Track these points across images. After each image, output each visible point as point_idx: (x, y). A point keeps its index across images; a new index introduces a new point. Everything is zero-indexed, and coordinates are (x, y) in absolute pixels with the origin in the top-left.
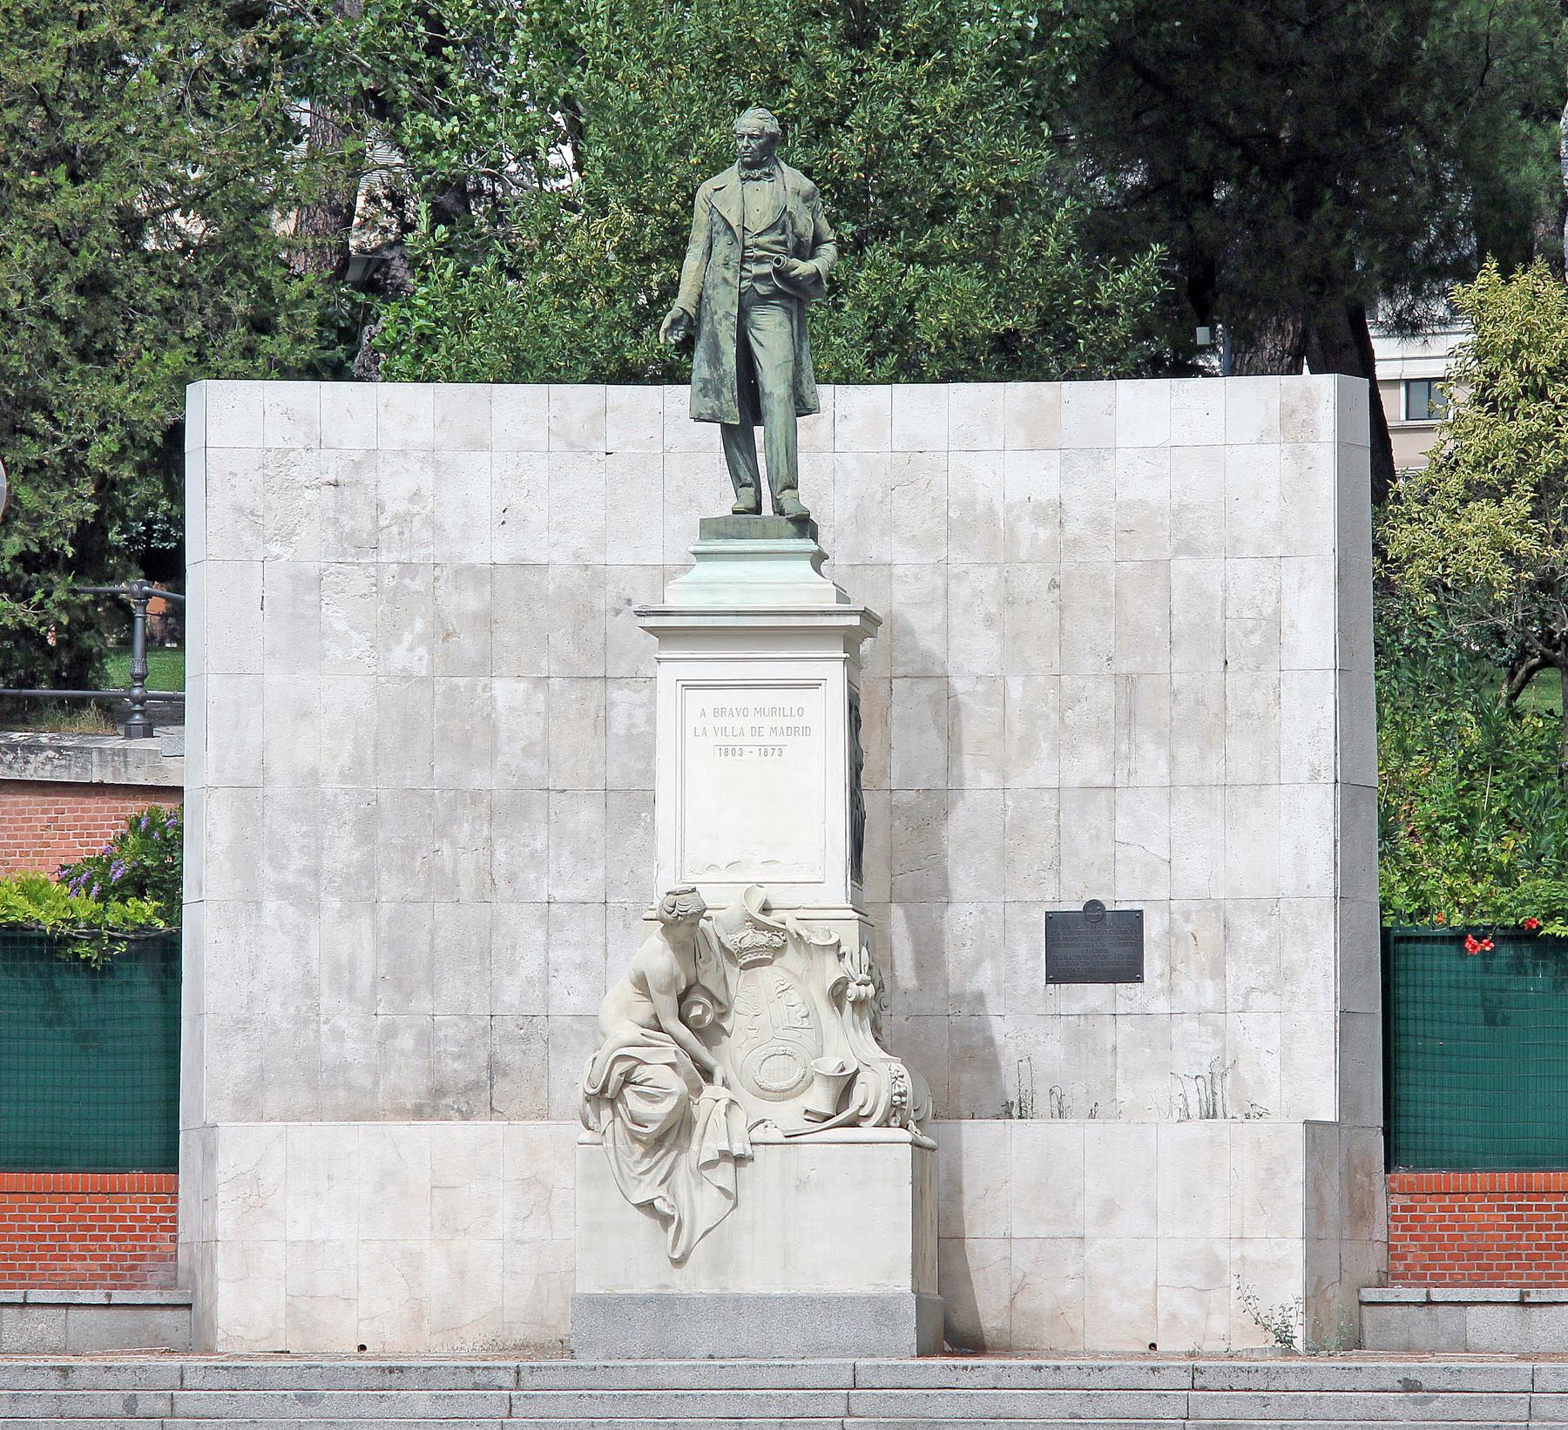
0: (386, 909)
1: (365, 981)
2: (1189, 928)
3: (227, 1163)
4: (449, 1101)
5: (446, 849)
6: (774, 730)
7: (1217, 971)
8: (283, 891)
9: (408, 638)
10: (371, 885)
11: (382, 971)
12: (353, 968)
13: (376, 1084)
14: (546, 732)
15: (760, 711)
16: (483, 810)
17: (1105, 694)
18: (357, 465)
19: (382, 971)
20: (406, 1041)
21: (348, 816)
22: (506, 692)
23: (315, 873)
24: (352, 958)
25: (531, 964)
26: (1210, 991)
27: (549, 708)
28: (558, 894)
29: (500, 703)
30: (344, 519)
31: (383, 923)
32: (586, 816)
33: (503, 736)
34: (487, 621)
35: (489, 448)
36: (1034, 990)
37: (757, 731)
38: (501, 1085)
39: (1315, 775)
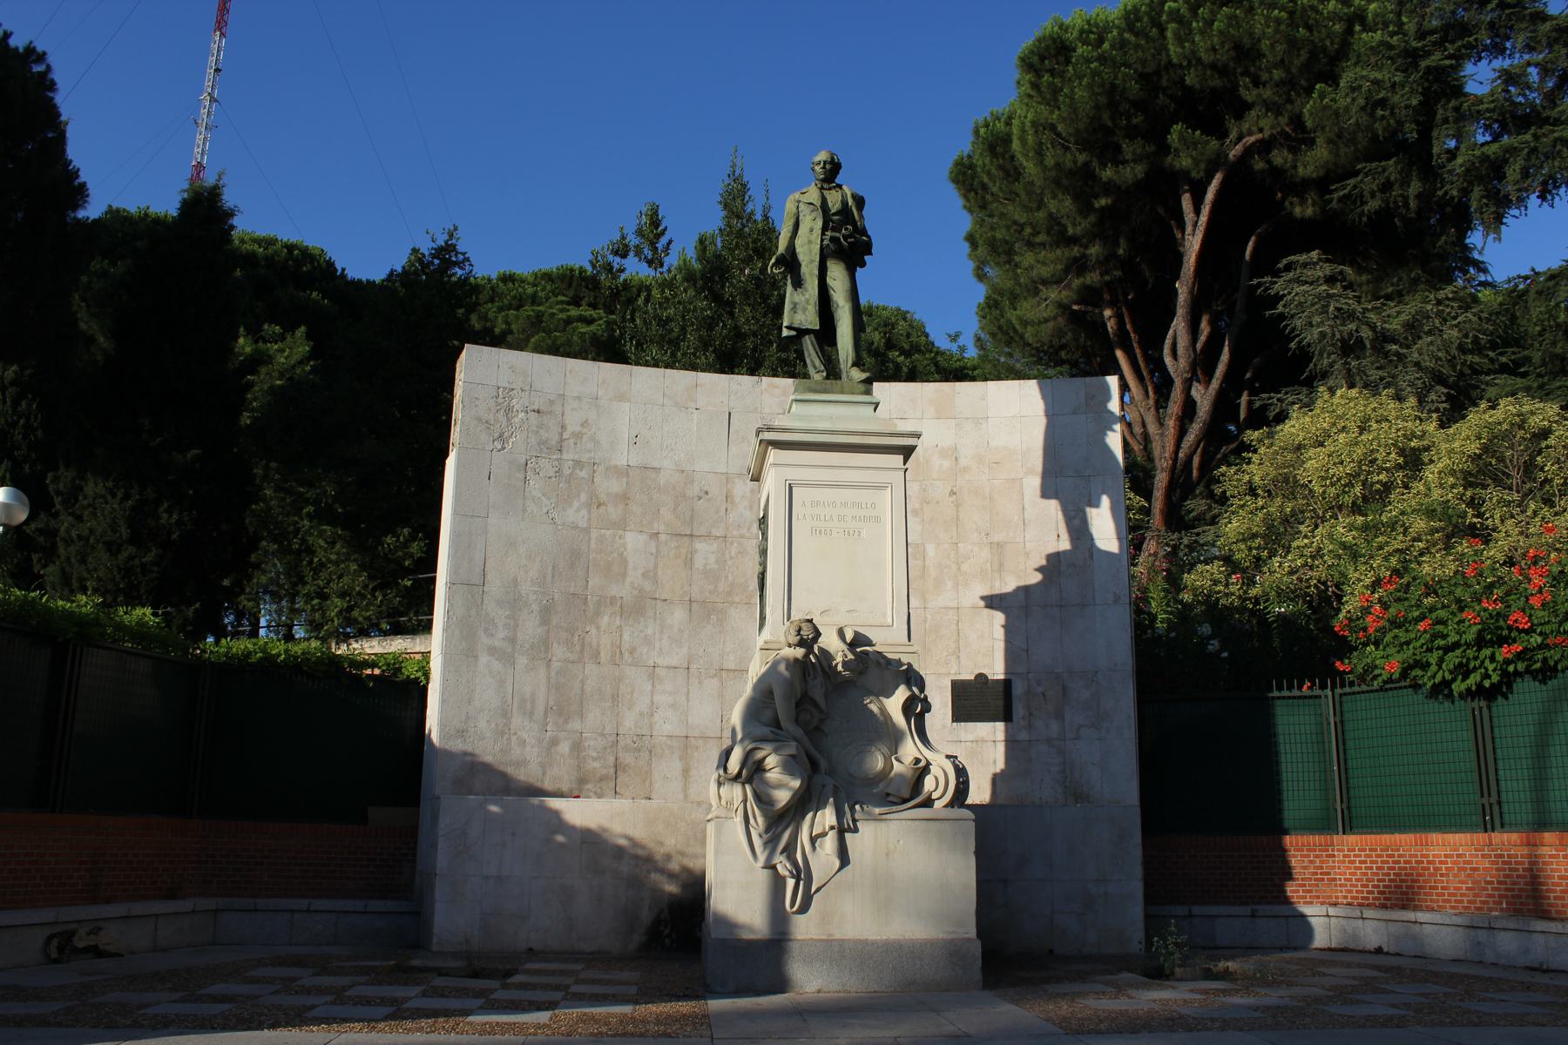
0: (555, 665)
1: (540, 709)
2: (1040, 689)
3: (444, 823)
4: (589, 786)
5: (594, 631)
6: (854, 518)
7: (1059, 715)
8: (492, 651)
9: (576, 504)
10: (547, 650)
11: (551, 703)
12: (533, 702)
13: (544, 773)
14: (656, 566)
15: (845, 504)
16: (617, 609)
17: (985, 554)
18: (552, 402)
19: (551, 703)
20: (564, 748)
21: (535, 607)
22: (633, 541)
23: (512, 641)
24: (533, 694)
25: (642, 704)
26: (1054, 728)
27: (658, 551)
28: (660, 661)
29: (630, 546)
30: (542, 432)
31: (553, 674)
32: (678, 615)
33: (630, 566)
34: (624, 498)
35: (629, 400)
36: (944, 727)
37: (842, 518)
38: (622, 777)
39: (1117, 599)
